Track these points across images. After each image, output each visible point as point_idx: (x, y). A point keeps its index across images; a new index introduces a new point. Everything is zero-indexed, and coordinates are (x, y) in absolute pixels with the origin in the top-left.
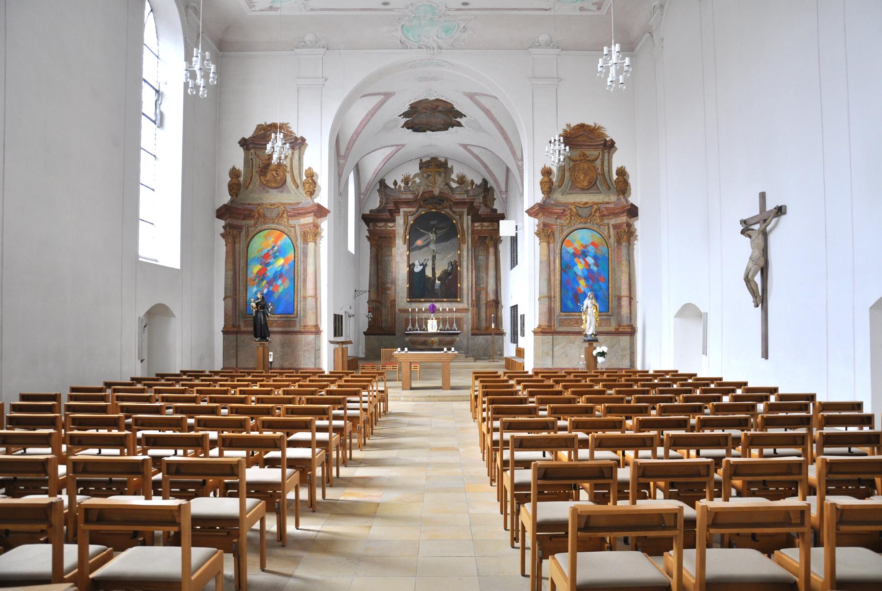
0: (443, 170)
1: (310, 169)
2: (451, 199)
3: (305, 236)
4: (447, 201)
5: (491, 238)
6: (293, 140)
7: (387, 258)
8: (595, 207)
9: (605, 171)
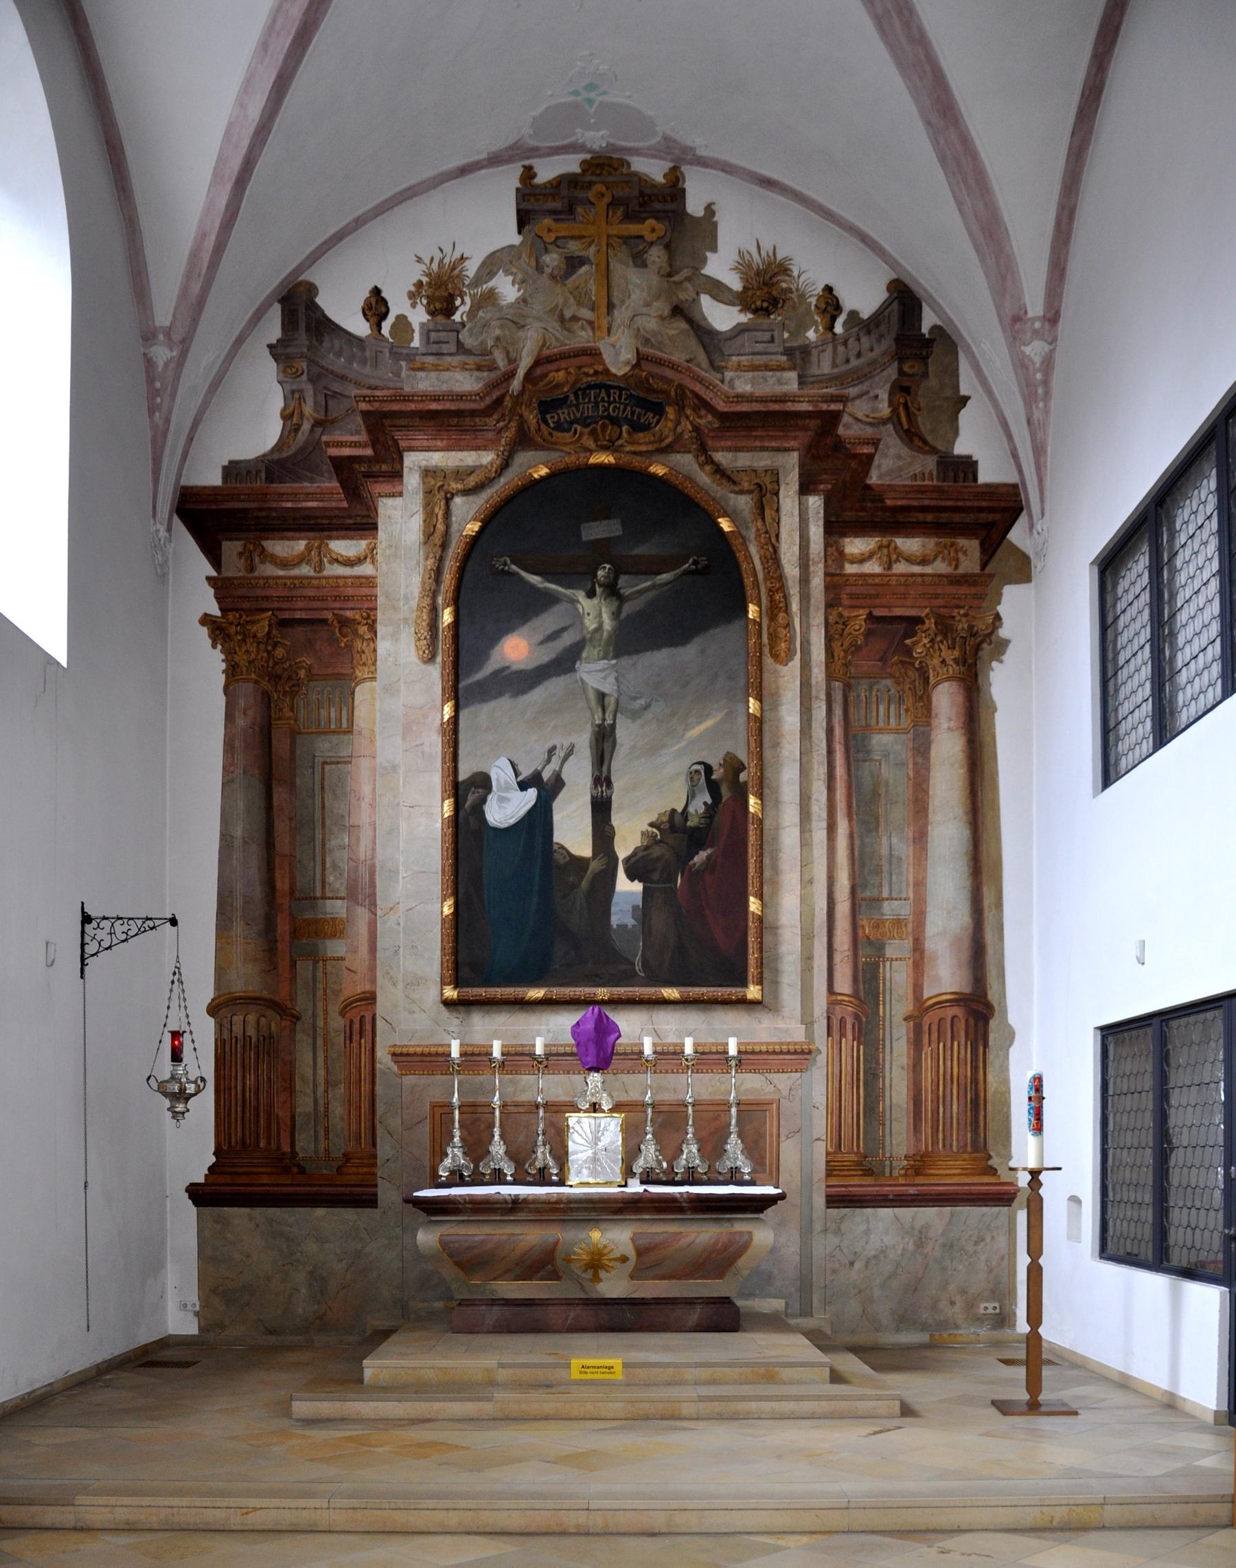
0: (660, 227)
2: (707, 395)
4: (681, 409)
5: (945, 628)
7: (323, 746)
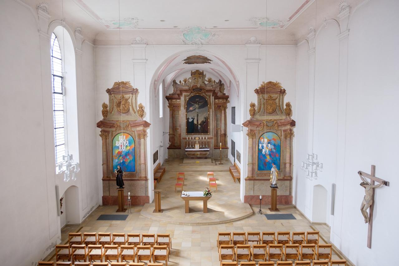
1: (141, 104)
3: (139, 136)
6: (132, 90)
8: (275, 122)
9: (280, 104)
